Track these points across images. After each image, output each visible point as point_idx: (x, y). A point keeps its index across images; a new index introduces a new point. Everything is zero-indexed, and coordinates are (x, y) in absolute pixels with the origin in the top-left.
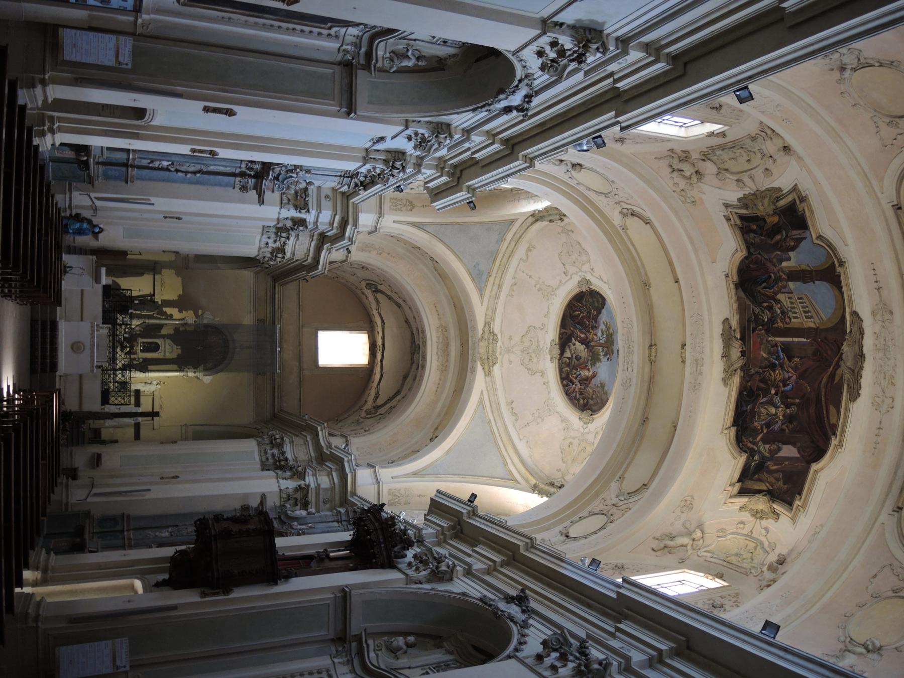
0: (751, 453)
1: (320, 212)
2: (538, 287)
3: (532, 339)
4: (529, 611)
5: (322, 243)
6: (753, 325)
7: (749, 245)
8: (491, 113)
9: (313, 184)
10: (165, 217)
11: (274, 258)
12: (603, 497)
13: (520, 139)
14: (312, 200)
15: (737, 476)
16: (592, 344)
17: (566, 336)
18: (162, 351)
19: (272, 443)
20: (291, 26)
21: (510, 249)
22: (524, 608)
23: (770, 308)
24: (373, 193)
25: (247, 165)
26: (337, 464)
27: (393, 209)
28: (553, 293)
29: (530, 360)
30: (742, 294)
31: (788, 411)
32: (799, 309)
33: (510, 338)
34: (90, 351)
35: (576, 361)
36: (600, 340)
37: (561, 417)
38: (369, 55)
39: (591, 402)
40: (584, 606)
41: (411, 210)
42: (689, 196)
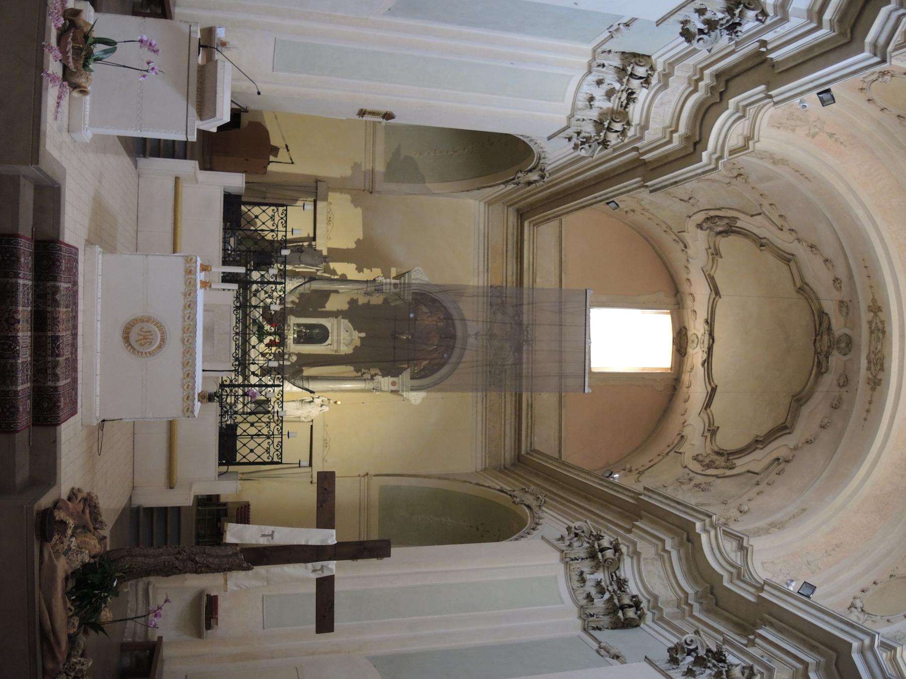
18: (332, 340)
34: (180, 349)
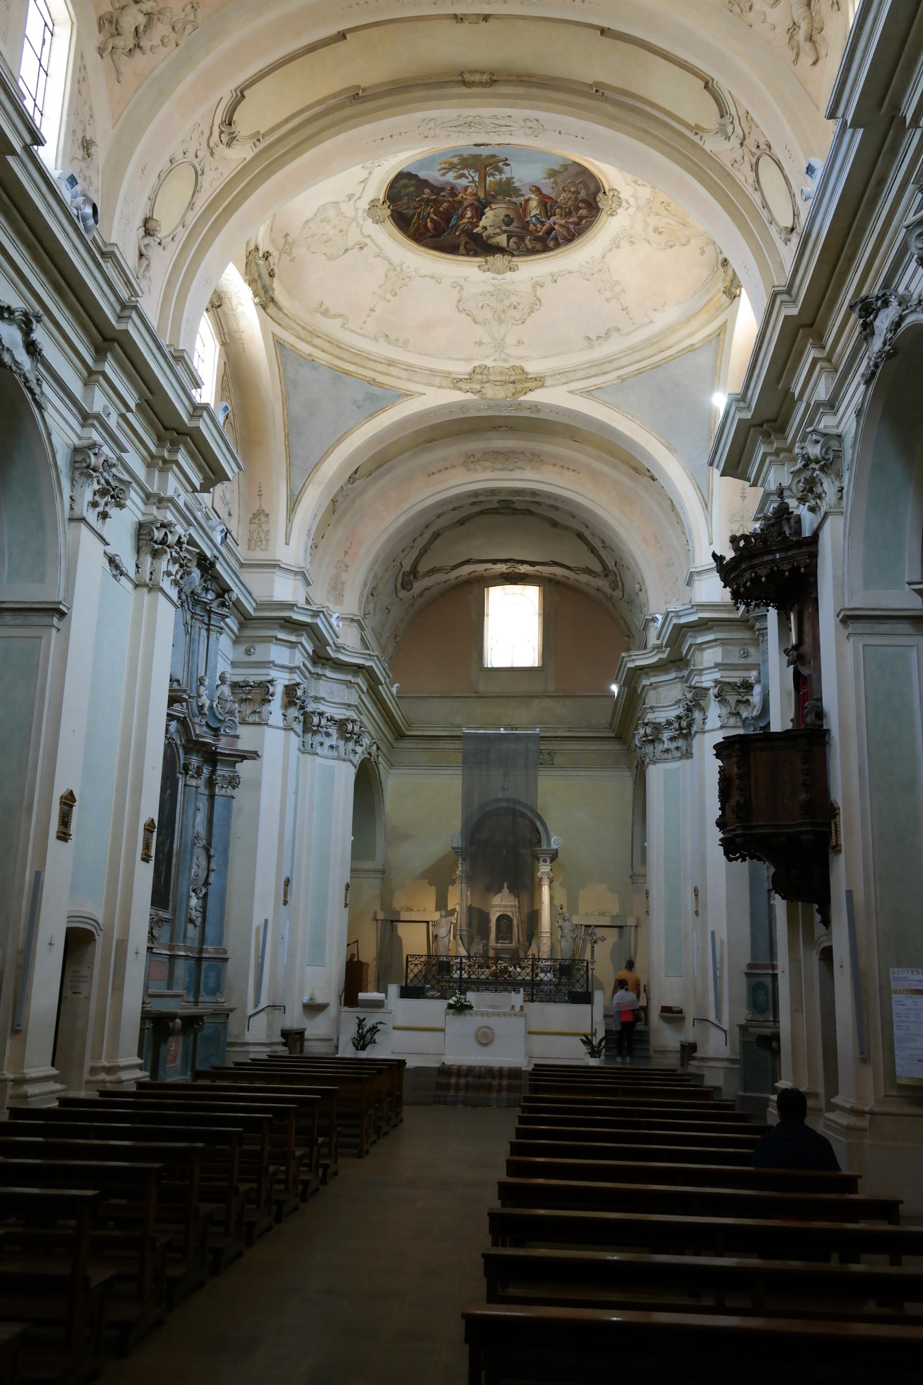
1: (273, 662)
2: (389, 296)
3: (480, 305)
4: (884, 295)
5: (327, 660)
8: (45, 379)
9: (223, 673)
10: (285, 903)
11: (355, 737)
12: (730, 166)
14: (254, 676)
16: (481, 195)
17: (472, 243)
19: (652, 741)
21: (327, 346)
22: (879, 303)
24: (234, 577)
25: (192, 777)
26: (685, 635)
27: (267, 545)
28: (398, 269)
29: (515, 308)
33: (480, 343)
35: (514, 224)
36: (473, 181)
37: (611, 250)
39: (583, 194)
40: (882, 191)
41: (268, 515)
42: (182, 15)
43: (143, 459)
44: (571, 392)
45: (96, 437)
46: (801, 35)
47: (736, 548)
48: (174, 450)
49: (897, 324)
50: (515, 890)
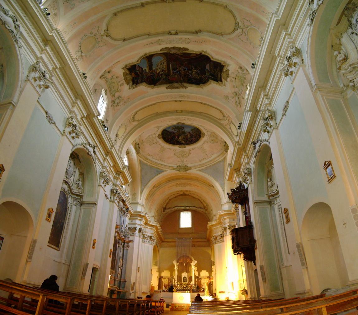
0: (209, 78)
2: (161, 152)
6: (167, 80)
7: (142, 82)
13: (106, 151)
14: (132, 226)
15: (216, 82)
20: (67, 219)
21: (149, 161)
23: (161, 75)
30: (158, 83)
31: (193, 68)
32: (161, 66)
38: (77, 195)
39: (198, 134)
43: (113, 177)
44: (197, 170)
45: (104, 170)
46: (238, 103)
47: (232, 191)
48: (119, 176)
49: (260, 146)
50: (187, 272)
